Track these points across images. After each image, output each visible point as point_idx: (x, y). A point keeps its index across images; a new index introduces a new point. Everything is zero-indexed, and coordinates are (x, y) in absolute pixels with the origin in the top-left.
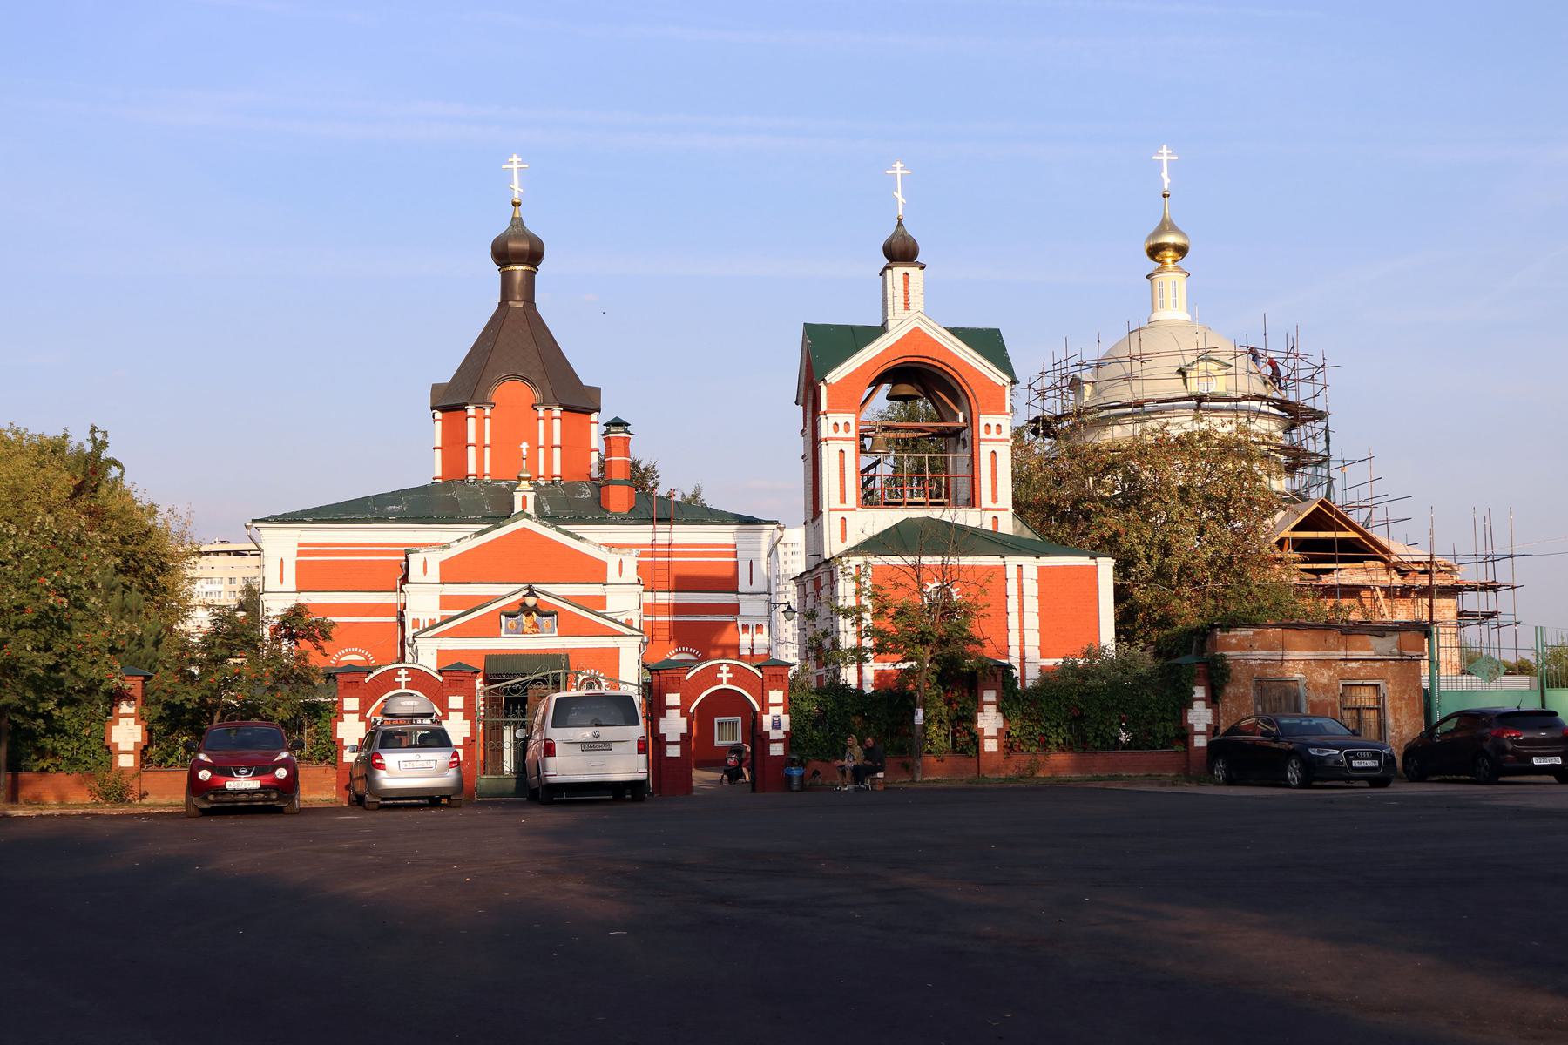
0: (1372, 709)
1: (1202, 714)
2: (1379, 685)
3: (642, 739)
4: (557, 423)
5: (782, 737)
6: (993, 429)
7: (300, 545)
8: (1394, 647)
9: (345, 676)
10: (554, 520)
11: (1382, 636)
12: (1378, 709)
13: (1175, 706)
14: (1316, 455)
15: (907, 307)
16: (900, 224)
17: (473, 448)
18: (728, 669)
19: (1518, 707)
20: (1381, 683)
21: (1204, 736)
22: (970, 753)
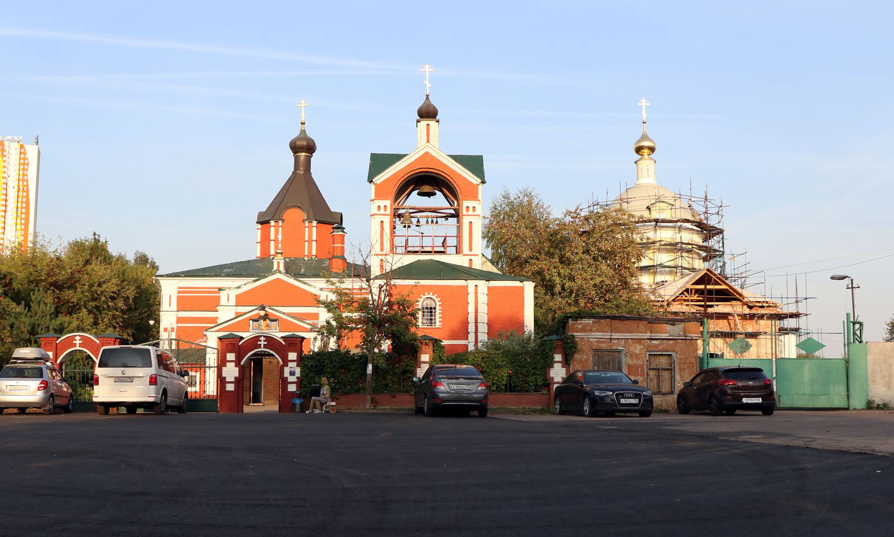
0: (667, 369)
2: (671, 355)
3: (153, 376)
4: (314, 229)
5: (296, 380)
6: (471, 209)
7: (179, 288)
9: (45, 339)
10: (297, 275)
11: (674, 325)
13: (543, 366)
14: (717, 251)
17: (273, 242)
18: (264, 339)
19: (739, 366)
20: (673, 354)
22: (411, 393)
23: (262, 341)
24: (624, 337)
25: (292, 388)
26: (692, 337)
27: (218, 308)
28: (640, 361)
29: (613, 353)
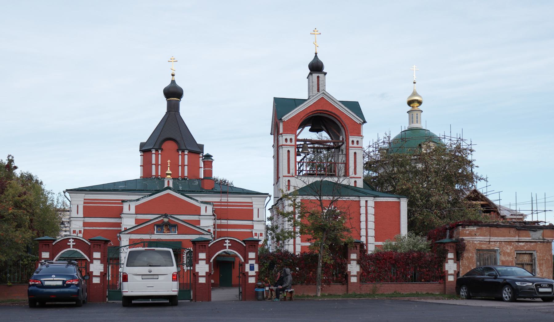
1: (452, 266)
2: (533, 253)
4: (186, 157)
5: (255, 274)
6: (355, 143)
7: (85, 200)
8: (540, 236)
12: (532, 265)
15: (318, 91)
16: (316, 56)
18: (229, 242)
21: (452, 276)
23: (227, 243)
24: (499, 240)
25: (252, 280)
26: (548, 240)
27: (122, 215)
28: (510, 258)
29: (491, 252)
